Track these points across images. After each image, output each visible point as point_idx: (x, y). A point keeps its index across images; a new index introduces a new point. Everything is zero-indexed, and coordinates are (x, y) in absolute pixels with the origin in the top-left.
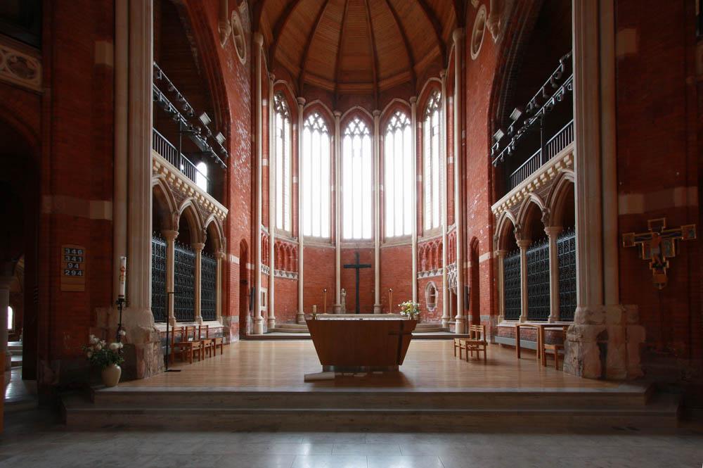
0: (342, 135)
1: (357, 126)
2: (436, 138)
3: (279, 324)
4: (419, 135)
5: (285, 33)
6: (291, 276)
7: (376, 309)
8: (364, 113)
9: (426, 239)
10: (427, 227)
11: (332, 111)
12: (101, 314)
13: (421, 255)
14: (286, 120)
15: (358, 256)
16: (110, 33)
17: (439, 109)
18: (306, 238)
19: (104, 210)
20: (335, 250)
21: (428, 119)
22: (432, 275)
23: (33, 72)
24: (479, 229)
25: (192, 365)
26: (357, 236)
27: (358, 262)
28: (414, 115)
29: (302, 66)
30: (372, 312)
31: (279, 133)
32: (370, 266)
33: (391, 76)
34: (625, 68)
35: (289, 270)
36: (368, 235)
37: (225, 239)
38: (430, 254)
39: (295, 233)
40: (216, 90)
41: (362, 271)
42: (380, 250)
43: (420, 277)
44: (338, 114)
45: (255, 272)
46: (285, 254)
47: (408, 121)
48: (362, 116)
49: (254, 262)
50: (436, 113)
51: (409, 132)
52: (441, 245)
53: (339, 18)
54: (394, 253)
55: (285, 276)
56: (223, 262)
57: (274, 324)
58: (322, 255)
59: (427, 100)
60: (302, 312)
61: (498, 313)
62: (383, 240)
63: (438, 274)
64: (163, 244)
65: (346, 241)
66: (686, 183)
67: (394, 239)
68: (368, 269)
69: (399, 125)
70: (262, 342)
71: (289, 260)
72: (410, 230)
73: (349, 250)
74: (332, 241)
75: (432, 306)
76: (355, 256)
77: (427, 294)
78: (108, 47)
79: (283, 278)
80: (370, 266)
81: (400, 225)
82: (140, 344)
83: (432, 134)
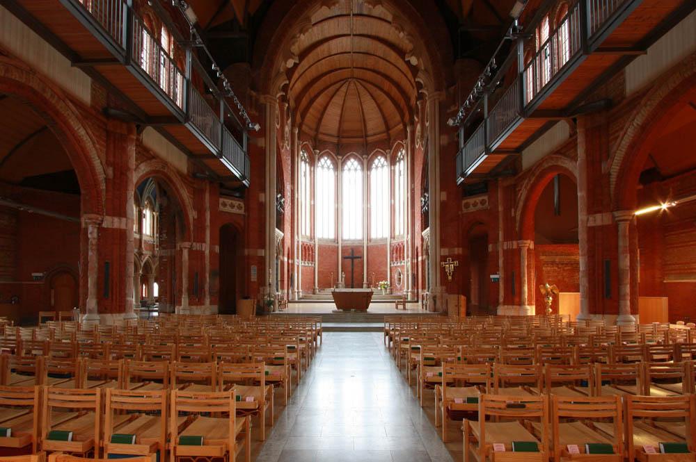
0: (342, 170)
1: (352, 165)
2: (402, 177)
4: (392, 173)
5: (308, 115)
7: (365, 286)
8: (357, 156)
9: (395, 242)
10: (397, 233)
11: (336, 156)
12: (261, 289)
13: (393, 251)
15: (353, 251)
16: (263, 190)
17: (403, 159)
18: (320, 240)
19: (261, 253)
20: (338, 247)
21: (398, 164)
22: (399, 264)
23: (242, 207)
24: (418, 243)
25: (228, 326)
26: (353, 237)
27: (353, 255)
28: (388, 158)
29: (317, 130)
30: (362, 288)
31: (303, 174)
32: (361, 258)
33: (375, 134)
34: (444, 205)
35: (309, 261)
36: (359, 237)
38: (398, 251)
39: (312, 238)
41: (356, 261)
42: (367, 247)
43: (392, 265)
44: (340, 157)
45: (293, 264)
46: (308, 251)
47: (385, 163)
48: (355, 158)
49: (293, 259)
50: (402, 162)
51: (386, 170)
52: (404, 247)
53: (345, 91)
54: (376, 250)
55: (307, 264)
57: (301, 294)
58: (329, 250)
59: (397, 153)
60: (317, 287)
61: (425, 289)
62: (369, 240)
63: (403, 264)
65: (345, 241)
66: (458, 247)
67: (376, 240)
68: (359, 259)
69: (380, 165)
70: (297, 304)
71: (309, 254)
72: (386, 234)
73: (347, 246)
74: (336, 241)
75: (399, 284)
76: (350, 251)
77: (396, 276)
78: (263, 195)
80: (361, 258)
81: (380, 231)
83: (400, 175)
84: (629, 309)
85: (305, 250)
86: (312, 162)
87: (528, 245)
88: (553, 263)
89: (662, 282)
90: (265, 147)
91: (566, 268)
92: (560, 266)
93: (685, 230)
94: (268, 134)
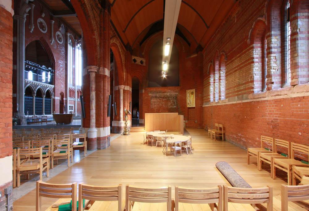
3: (78, 115)
6: (73, 100)
14: (71, 46)
37: (54, 93)
40: (231, 72)
49: (66, 97)
55: (71, 99)
56: (53, 99)
64: (32, 98)
79: (71, 100)
82: (21, 119)
84: (94, 125)
85: (70, 91)
86: (74, 46)
87: (123, 88)
88: (156, 97)
89: (201, 106)
90: (17, 42)
91: (163, 100)
92: (160, 99)
93: (102, 87)
94: (18, 35)
